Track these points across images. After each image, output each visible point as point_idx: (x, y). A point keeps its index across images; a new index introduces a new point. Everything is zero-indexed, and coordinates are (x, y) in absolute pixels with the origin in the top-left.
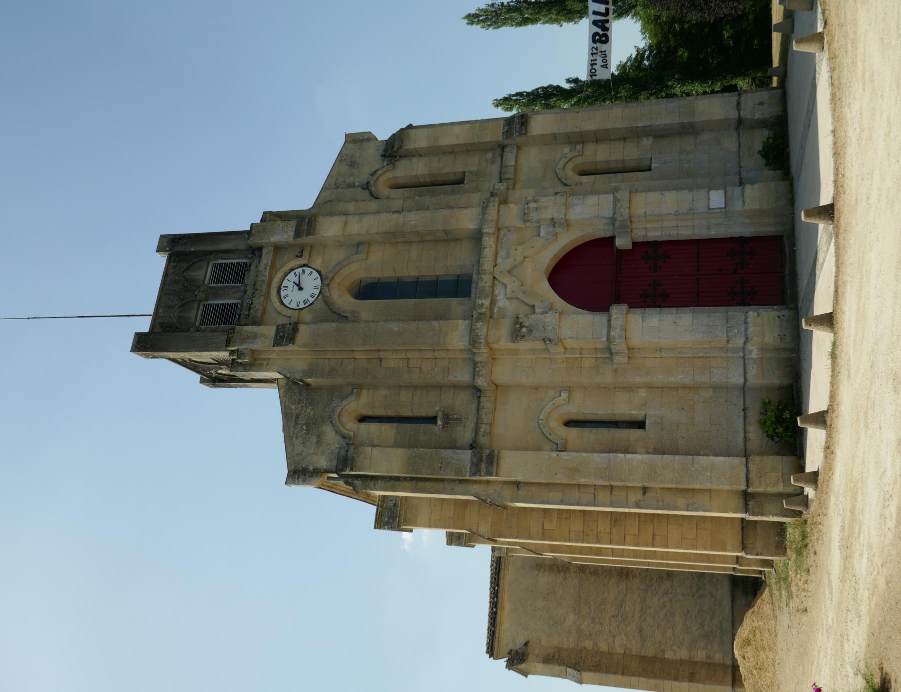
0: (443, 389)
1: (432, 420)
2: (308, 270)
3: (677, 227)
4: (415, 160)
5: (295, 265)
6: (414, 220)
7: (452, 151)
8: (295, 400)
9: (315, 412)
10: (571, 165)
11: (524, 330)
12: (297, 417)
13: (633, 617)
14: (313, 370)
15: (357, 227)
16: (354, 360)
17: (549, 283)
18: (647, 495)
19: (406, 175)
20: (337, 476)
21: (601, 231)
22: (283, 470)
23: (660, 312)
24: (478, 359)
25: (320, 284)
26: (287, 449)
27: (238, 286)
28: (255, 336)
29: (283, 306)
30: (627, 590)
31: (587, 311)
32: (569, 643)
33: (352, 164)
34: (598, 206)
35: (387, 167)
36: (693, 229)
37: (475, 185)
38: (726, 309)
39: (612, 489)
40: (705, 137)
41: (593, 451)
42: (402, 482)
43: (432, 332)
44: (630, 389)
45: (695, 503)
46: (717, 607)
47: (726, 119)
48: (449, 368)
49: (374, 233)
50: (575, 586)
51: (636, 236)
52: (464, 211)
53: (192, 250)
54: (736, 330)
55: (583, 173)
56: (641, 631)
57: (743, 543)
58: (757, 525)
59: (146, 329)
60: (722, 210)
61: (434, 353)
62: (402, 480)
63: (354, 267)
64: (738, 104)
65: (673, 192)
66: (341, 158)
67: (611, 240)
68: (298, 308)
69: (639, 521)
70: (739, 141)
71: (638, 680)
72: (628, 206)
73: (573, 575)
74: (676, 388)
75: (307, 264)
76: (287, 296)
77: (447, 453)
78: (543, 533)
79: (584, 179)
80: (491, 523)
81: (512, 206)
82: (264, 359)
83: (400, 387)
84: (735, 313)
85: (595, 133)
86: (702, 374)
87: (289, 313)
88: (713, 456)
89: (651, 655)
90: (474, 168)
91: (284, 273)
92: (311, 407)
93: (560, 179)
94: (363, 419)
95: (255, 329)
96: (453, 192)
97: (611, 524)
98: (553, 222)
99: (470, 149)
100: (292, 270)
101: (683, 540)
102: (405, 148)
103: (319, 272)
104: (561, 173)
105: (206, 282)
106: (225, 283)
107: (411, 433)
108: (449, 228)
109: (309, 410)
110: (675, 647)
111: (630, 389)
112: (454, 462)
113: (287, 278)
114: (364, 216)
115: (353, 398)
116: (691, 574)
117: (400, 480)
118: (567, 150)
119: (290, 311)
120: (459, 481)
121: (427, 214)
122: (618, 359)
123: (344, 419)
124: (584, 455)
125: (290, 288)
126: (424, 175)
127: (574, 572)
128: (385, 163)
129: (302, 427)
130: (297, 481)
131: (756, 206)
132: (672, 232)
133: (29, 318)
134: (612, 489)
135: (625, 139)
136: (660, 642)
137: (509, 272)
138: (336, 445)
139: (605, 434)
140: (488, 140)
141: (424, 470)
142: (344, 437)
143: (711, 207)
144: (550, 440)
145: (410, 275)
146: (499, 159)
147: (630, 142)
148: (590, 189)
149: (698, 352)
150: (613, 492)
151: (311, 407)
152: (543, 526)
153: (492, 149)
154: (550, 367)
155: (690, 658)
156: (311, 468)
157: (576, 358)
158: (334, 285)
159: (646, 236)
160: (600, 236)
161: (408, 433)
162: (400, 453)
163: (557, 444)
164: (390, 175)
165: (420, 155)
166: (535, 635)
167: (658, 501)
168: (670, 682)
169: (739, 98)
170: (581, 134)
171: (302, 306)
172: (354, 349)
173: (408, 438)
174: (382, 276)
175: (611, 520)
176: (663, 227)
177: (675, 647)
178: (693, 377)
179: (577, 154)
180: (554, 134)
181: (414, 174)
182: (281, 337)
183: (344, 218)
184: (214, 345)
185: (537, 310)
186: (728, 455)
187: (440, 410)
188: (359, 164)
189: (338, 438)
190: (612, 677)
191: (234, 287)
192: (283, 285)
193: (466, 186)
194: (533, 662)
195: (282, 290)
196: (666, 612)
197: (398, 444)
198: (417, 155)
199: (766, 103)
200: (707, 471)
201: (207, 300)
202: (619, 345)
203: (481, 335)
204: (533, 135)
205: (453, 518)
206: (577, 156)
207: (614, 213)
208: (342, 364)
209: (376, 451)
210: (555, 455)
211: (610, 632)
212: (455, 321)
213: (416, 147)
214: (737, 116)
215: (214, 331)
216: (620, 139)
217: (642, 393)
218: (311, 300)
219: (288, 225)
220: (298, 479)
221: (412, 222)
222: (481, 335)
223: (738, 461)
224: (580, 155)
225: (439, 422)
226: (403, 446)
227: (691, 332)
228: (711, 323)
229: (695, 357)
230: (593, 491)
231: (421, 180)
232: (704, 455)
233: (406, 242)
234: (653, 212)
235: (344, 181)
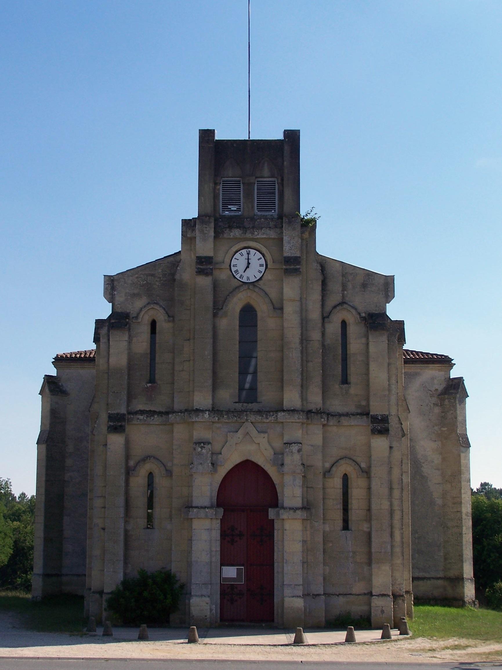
2: (263, 269)
12: (153, 275)
22: (113, 272)
29: (234, 253)
33: (364, 286)
66: (369, 274)
87: (227, 260)
100: (263, 255)
103: (261, 279)
109: (157, 284)
113: (257, 252)
115: (166, 318)
119: (229, 261)
123: (151, 313)
128: (363, 315)
130: (106, 283)
131: (286, 605)
138: (132, 309)
142: (138, 314)
151: (160, 285)
155: (64, 538)
156: (115, 293)
162: (123, 361)
171: (233, 269)
188: (364, 291)
195: (247, 250)
201: (243, 183)
203: (198, 418)
208: (187, 309)
209: (125, 344)
218: (238, 277)
219: (297, 250)
220: (107, 284)
221: (291, 355)
222: (198, 418)
226: (129, 362)
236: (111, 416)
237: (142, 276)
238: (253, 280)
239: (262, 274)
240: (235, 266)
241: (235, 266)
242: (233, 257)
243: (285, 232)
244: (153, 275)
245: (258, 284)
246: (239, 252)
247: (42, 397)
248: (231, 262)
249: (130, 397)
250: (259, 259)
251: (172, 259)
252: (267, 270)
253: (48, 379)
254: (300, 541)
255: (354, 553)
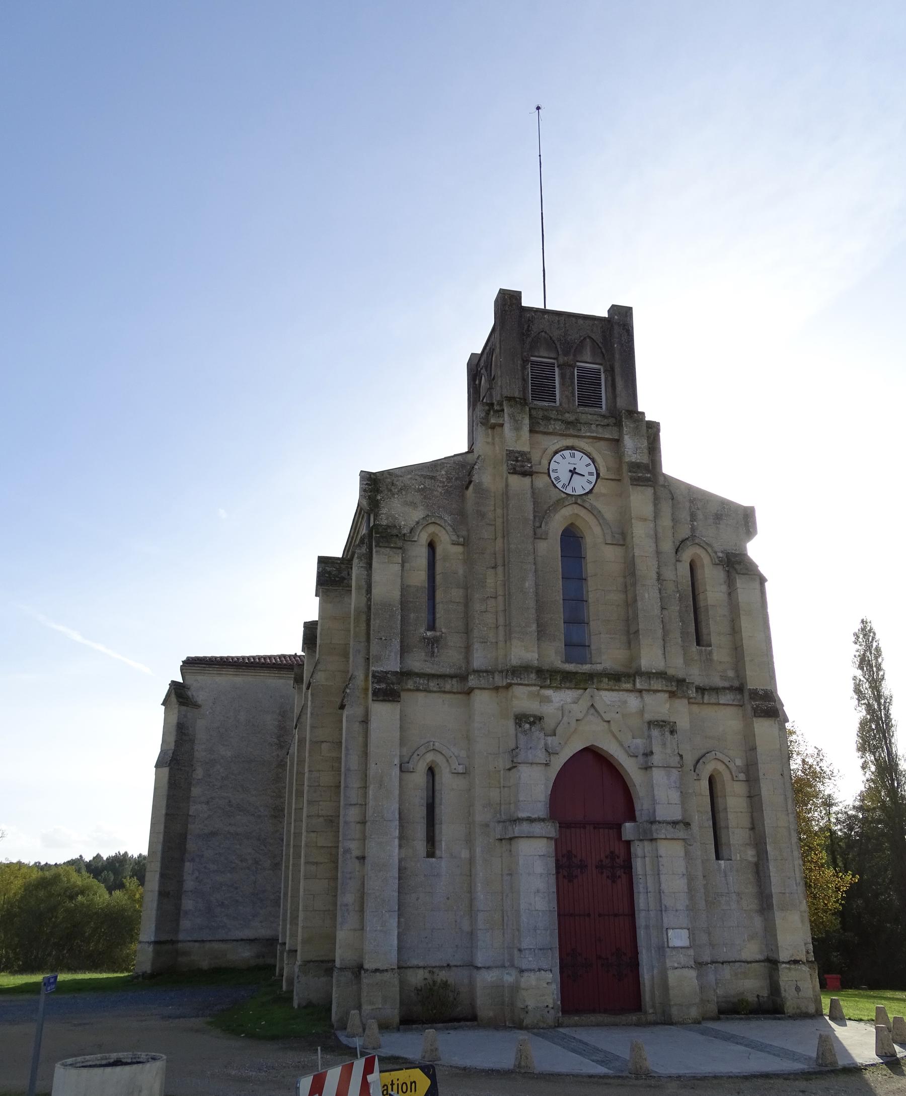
0: (465, 634)
1: (432, 627)
2: (593, 479)
3: (647, 893)
4: (724, 588)
5: (598, 465)
6: (649, 598)
7: (735, 630)
8: (450, 474)
9: (437, 497)
10: (721, 767)
11: (527, 726)
13: (230, 824)
14: (482, 494)
15: (640, 532)
16: (494, 538)
17: (584, 748)
18: (357, 861)
19: (706, 580)
20: (371, 526)
21: (642, 806)
23: (550, 874)
24: (496, 675)
25: (577, 493)
26: (398, 469)
27: (575, 401)
28: (517, 429)
30: (259, 816)
31: (550, 793)
32: (200, 752)
34: (668, 804)
35: (716, 557)
36: (645, 910)
37: (696, 658)
38: (556, 948)
39: (363, 823)
40: (758, 922)
41: (401, 802)
42: (366, 597)
43: (524, 625)
44: (469, 841)
45: (349, 914)
46: (242, 922)
47: (777, 947)
48: (487, 642)
49: (634, 553)
50: (262, 757)
51: (636, 845)
52: (660, 652)
53: (615, 346)
54: (532, 959)
55: (711, 780)
56: (213, 834)
57: (309, 962)
58: (329, 978)
59: (525, 303)
60: (666, 943)
61: (502, 626)
62: (368, 597)
63: (597, 530)
64: (796, 962)
65: (686, 887)
67: (632, 817)
68: (551, 471)
69: (331, 847)
70: (754, 962)
71: (160, 833)
72: (668, 837)
73: (274, 754)
74: (471, 891)
75: (601, 478)
76: (564, 458)
77: (396, 644)
78: (317, 742)
79: (705, 784)
80: (326, 685)
81: (668, 706)
82: (493, 439)
83: (466, 588)
84: (550, 958)
85: (759, 795)
86: (485, 920)
87: (545, 462)
88: (398, 933)
89: (187, 846)
90: (715, 657)
91: (589, 453)
92: (443, 492)
93: (704, 756)
94: (431, 546)
95: (526, 429)
96: (684, 634)
97: (327, 816)
98: (649, 754)
99: (737, 651)
100: (594, 462)
101: (312, 896)
102: (737, 577)
103: (591, 491)
104: (711, 756)
105: (578, 364)
106: (578, 391)
107: (417, 603)
108: (641, 637)
109: (440, 490)
110: (197, 874)
111: (469, 841)
112: (387, 652)
114: (654, 540)
116: (278, 891)
117: (367, 594)
118: (739, 762)
120: (368, 659)
121: (657, 611)
122: (499, 828)
124: (397, 792)
125: (572, 460)
126: (706, 599)
127: (278, 755)
128: (720, 555)
129: (422, 484)
130: (365, 483)
132: (641, 886)
133: (540, 156)
134: (363, 823)
135: (753, 829)
136: (202, 856)
137: (592, 705)
138: (403, 523)
139: (419, 813)
140: (747, 673)
141: (378, 622)
143: (669, 930)
144: (413, 755)
145: (590, 593)
146: (726, 684)
147: (750, 835)
148: (690, 791)
149: (508, 916)
150: (359, 825)
152: (325, 742)
153: (738, 676)
154: (490, 754)
155: (185, 891)
157: (499, 782)
158: (576, 509)
159: (636, 857)
160: (635, 805)
161: (417, 600)
163: (409, 763)
164: (706, 560)
165: (730, 594)
166: (208, 712)
167: (350, 873)
168: (159, 869)
169: (803, 963)
170: (757, 780)
171: (553, 475)
172: (505, 538)
173: (411, 600)
174: (588, 561)
175: (331, 816)
176: (646, 877)
177: (197, 874)
178: (482, 911)
179: (734, 774)
180: (756, 748)
181: (708, 588)
182: (517, 458)
183: (651, 517)
184: (508, 381)
185: (549, 739)
186: (400, 949)
187: (442, 633)
189: (412, 524)
190: (164, 803)
191: (573, 396)
192: (576, 452)
193: (694, 648)
194: (179, 711)
195: (570, 451)
196: (235, 863)
197: (404, 589)
198: (730, 591)
199: (798, 995)
200: (382, 926)
202: (517, 830)
204: (753, 724)
205: (331, 643)
206: (732, 774)
207: (659, 822)
209: (397, 568)
210: (396, 763)
211: (212, 798)
212: (536, 649)
213: (739, 590)
214: (781, 959)
215: (524, 380)
216: (753, 823)
217: (465, 854)
220: (367, 484)
221: (647, 595)
223: (393, 959)
224: (733, 778)
225: (429, 633)
227: (529, 910)
228: (539, 932)
229: (503, 913)
230: (360, 802)
231: (701, 597)
232: (399, 922)
233: (626, 586)
234: (663, 865)
235: (698, 509)
236: (377, 674)
237: (417, 477)
238: (580, 492)
239: (592, 486)
240: (555, 471)
241: (555, 471)
242: (552, 458)
243: (626, 429)
244: (432, 478)
245: (588, 498)
246: (560, 453)
247: (165, 708)
248: (549, 466)
249: (404, 650)
250: (587, 465)
251: (460, 458)
252: (599, 480)
253: (174, 684)
254: (683, 875)
255: (738, 894)
